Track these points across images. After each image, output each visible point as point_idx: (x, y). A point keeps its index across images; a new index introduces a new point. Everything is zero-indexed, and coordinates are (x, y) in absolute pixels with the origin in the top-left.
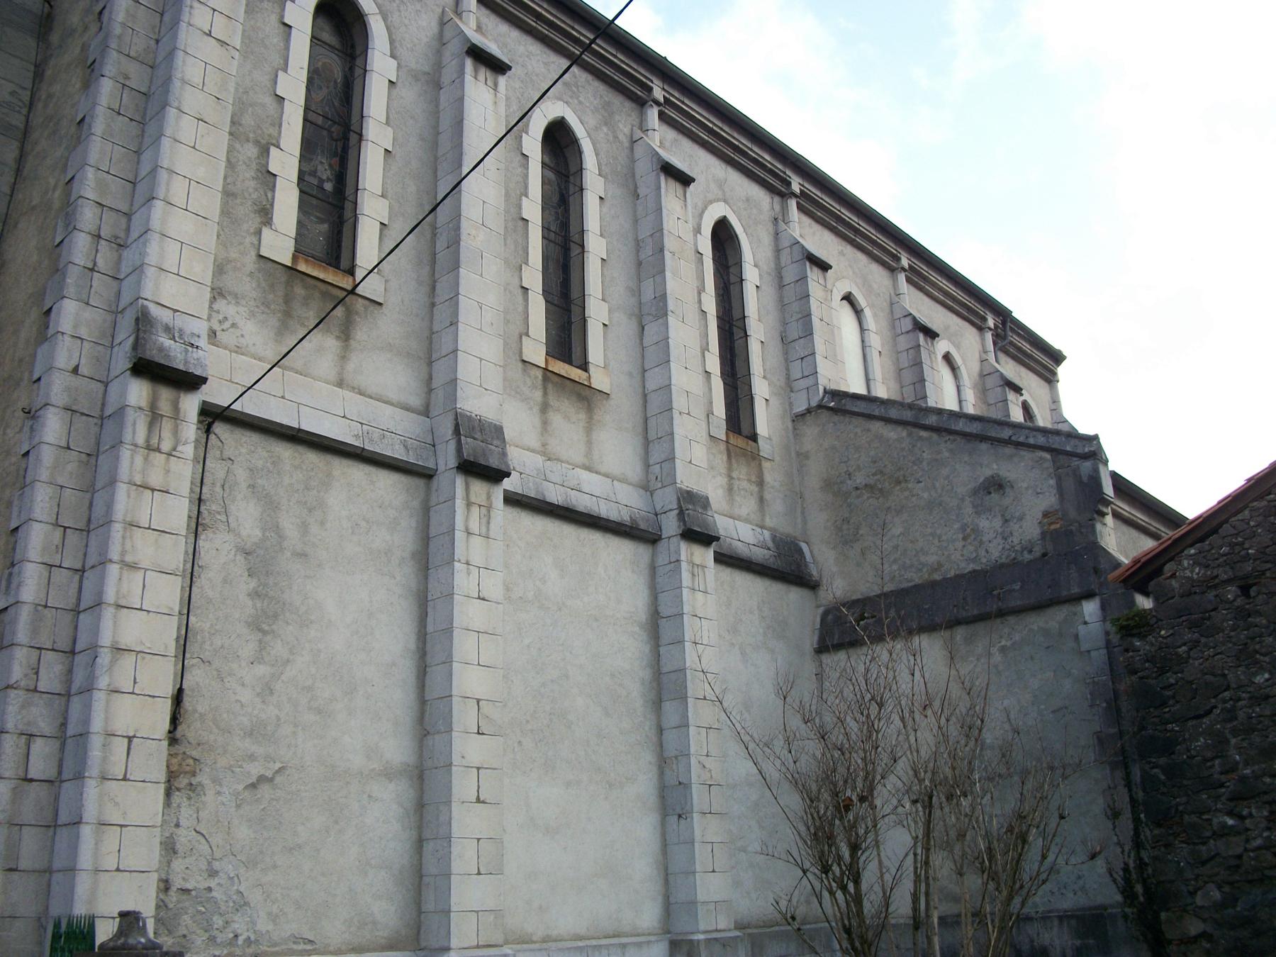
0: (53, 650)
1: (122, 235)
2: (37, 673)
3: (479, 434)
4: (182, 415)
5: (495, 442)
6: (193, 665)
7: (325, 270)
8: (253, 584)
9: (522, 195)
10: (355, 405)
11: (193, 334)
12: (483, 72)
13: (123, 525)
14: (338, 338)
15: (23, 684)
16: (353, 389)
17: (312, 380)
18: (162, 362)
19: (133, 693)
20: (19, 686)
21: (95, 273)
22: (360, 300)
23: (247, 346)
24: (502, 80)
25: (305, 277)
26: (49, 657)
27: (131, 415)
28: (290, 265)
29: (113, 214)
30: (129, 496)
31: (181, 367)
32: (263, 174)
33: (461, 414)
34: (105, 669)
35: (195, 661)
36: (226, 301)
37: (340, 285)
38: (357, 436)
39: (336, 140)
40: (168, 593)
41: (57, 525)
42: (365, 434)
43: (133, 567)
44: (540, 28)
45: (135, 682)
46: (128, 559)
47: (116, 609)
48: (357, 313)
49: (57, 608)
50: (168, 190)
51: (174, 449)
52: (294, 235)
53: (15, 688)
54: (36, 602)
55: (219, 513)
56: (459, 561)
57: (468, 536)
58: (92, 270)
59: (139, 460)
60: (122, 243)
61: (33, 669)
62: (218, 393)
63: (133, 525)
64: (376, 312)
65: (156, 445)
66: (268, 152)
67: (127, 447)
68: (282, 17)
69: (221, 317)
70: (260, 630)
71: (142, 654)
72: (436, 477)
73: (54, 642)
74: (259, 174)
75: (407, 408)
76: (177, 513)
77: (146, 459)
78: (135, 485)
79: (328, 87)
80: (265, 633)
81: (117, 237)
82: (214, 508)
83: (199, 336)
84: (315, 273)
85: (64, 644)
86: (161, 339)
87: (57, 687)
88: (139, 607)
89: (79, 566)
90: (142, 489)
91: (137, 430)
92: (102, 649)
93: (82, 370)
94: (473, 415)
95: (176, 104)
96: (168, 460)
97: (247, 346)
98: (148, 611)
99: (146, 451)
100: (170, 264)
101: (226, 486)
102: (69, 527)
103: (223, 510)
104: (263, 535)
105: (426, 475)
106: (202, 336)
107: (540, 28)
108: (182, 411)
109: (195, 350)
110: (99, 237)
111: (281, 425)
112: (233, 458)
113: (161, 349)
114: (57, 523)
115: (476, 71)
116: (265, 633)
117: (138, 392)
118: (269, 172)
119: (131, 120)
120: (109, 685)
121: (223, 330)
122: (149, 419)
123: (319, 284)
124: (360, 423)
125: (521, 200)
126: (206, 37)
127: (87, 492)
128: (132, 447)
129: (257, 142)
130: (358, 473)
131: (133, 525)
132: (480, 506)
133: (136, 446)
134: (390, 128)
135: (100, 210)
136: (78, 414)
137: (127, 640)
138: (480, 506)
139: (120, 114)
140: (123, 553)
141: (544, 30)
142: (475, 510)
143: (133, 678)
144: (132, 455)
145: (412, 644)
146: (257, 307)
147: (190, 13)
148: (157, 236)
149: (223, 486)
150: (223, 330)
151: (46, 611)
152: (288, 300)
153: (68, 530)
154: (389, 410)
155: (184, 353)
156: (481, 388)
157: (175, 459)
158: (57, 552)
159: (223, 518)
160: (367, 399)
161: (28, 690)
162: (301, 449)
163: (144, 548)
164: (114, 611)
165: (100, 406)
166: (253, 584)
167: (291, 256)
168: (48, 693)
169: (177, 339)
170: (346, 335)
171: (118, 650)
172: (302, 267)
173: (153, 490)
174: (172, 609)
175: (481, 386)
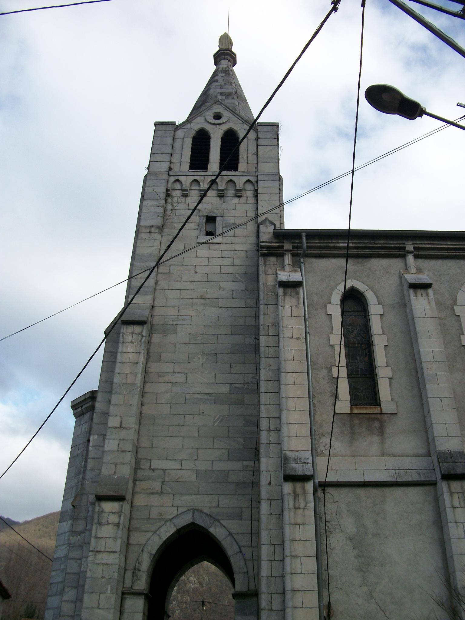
0: (276, 593)
1: (278, 426)
2: (271, 603)
3: (450, 459)
4: (306, 492)
5: (460, 461)
6: (334, 591)
7: (366, 408)
8: (356, 552)
9: (460, 334)
10: (390, 462)
11: (305, 458)
12: (419, 292)
13: (289, 541)
14: (378, 435)
15: (267, 608)
16: (389, 455)
17: (369, 458)
18: (293, 474)
19: (302, 607)
20: (265, 609)
21: (271, 444)
22: (386, 415)
23: (338, 452)
24: (430, 291)
25: (358, 415)
26: (275, 596)
27: (286, 498)
28: (350, 413)
29: (273, 419)
30: (290, 529)
31: (301, 474)
32: (331, 380)
33: (439, 453)
34: (290, 599)
35: (334, 589)
36: (325, 437)
37: (374, 412)
38: (393, 476)
39: (365, 350)
40: (311, 565)
41: (271, 544)
42: (397, 474)
43: (296, 557)
44: (450, 254)
45: (303, 603)
46: (293, 554)
47: (291, 574)
48: (385, 422)
49: (275, 577)
50: (287, 405)
51: (306, 506)
52: (349, 399)
53: (264, 610)
54: (268, 576)
55: (336, 525)
56: (451, 522)
57: (453, 510)
58: (269, 444)
59: (292, 514)
60: (279, 430)
61: (270, 601)
62: (320, 478)
63: (293, 540)
64: (394, 418)
65: (298, 507)
66: (331, 370)
67: (287, 510)
68: (327, 312)
69: (324, 444)
70: (362, 571)
71: (304, 591)
72: (437, 484)
73: (276, 590)
74: (330, 380)
75: (418, 456)
76: (310, 532)
77: (295, 513)
78: (292, 524)
79: (357, 329)
80: (365, 572)
81: (276, 428)
82: (334, 523)
83: (308, 458)
84: (362, 412)
85: (280, 590)
86: (292, 465)
87: (279, 607)
88: (300, 572)
89: (281, 559)
90: (295, 525)
91: (289, 502)
92: (288, 592)
93: (272, 483)
94: (446, 451)
95: (284, 371)
96: (304, 511)
97: (338, 452)
98: (304, 573)
99: (294, 510)
100: (293, 434)
101: (338, 514)
102: (276, 544)
103: (338, 523)
104: (358, 530)
105: (433, 484)
106: (309, 458)
107: (450, 254)
108: (306, 490)
109: (307, 465)
110: (270, 430)
111: (356, 482)
112: (338, 501)
113: (292, 469)
114: (271, 544)
115: (416, 293)
116: (365, 572)
117: (288, 487)
118: (333, 378)
119: (274, 381)
120: (292, 605)
121: (326, 449)
122: (293, 497)
123: (364, 415)
124: (394, 470)
125: (460, 337)
126: (291, 339)
127: (281, 529)
128: (289, 510)
129: (326, 368)
130: (398, 492)
131: (293, 540)
132: (458, 493)
133: (290, 509)
134: (385, 335)
135: (269, 420)
136: (273, 500)
137: (297, 586)
138: (458, 493)
139: (270, 381)
140: (291, 552)
141: (453, 253)
142: (456, 496)
143: (301, 601)
144: (289, 512)
145: (440, 565)
146: (339, 435)
147: (283, 333)
148: (285, 425)
149: (336, 514)
150: (326, 449)
151: (272, 578)
152: (352, 427)
153: (276, 546)
154: (408, 460)
155: (302, 468)
156: (448, 437)
157: (307, 510)
158: (273, 554)
159: (338, 527)
160: (398, 458)
161: (269, 610)
162: (369, 489)
163: (299, 548)
164: (290, 576)
165: (281, 494)
166: (356, 552)
167: (349, 408)
168: (277, 610)
169: (299, 463)
170: (381, 432)
171: (294, 591)
172: (356, 411)
173: (299, 525)
174: (314, 571)
175: (448, 436)
